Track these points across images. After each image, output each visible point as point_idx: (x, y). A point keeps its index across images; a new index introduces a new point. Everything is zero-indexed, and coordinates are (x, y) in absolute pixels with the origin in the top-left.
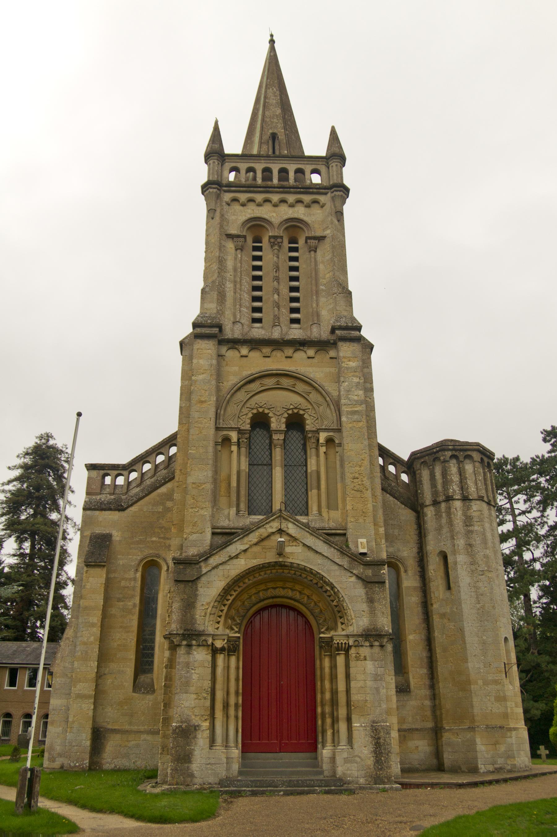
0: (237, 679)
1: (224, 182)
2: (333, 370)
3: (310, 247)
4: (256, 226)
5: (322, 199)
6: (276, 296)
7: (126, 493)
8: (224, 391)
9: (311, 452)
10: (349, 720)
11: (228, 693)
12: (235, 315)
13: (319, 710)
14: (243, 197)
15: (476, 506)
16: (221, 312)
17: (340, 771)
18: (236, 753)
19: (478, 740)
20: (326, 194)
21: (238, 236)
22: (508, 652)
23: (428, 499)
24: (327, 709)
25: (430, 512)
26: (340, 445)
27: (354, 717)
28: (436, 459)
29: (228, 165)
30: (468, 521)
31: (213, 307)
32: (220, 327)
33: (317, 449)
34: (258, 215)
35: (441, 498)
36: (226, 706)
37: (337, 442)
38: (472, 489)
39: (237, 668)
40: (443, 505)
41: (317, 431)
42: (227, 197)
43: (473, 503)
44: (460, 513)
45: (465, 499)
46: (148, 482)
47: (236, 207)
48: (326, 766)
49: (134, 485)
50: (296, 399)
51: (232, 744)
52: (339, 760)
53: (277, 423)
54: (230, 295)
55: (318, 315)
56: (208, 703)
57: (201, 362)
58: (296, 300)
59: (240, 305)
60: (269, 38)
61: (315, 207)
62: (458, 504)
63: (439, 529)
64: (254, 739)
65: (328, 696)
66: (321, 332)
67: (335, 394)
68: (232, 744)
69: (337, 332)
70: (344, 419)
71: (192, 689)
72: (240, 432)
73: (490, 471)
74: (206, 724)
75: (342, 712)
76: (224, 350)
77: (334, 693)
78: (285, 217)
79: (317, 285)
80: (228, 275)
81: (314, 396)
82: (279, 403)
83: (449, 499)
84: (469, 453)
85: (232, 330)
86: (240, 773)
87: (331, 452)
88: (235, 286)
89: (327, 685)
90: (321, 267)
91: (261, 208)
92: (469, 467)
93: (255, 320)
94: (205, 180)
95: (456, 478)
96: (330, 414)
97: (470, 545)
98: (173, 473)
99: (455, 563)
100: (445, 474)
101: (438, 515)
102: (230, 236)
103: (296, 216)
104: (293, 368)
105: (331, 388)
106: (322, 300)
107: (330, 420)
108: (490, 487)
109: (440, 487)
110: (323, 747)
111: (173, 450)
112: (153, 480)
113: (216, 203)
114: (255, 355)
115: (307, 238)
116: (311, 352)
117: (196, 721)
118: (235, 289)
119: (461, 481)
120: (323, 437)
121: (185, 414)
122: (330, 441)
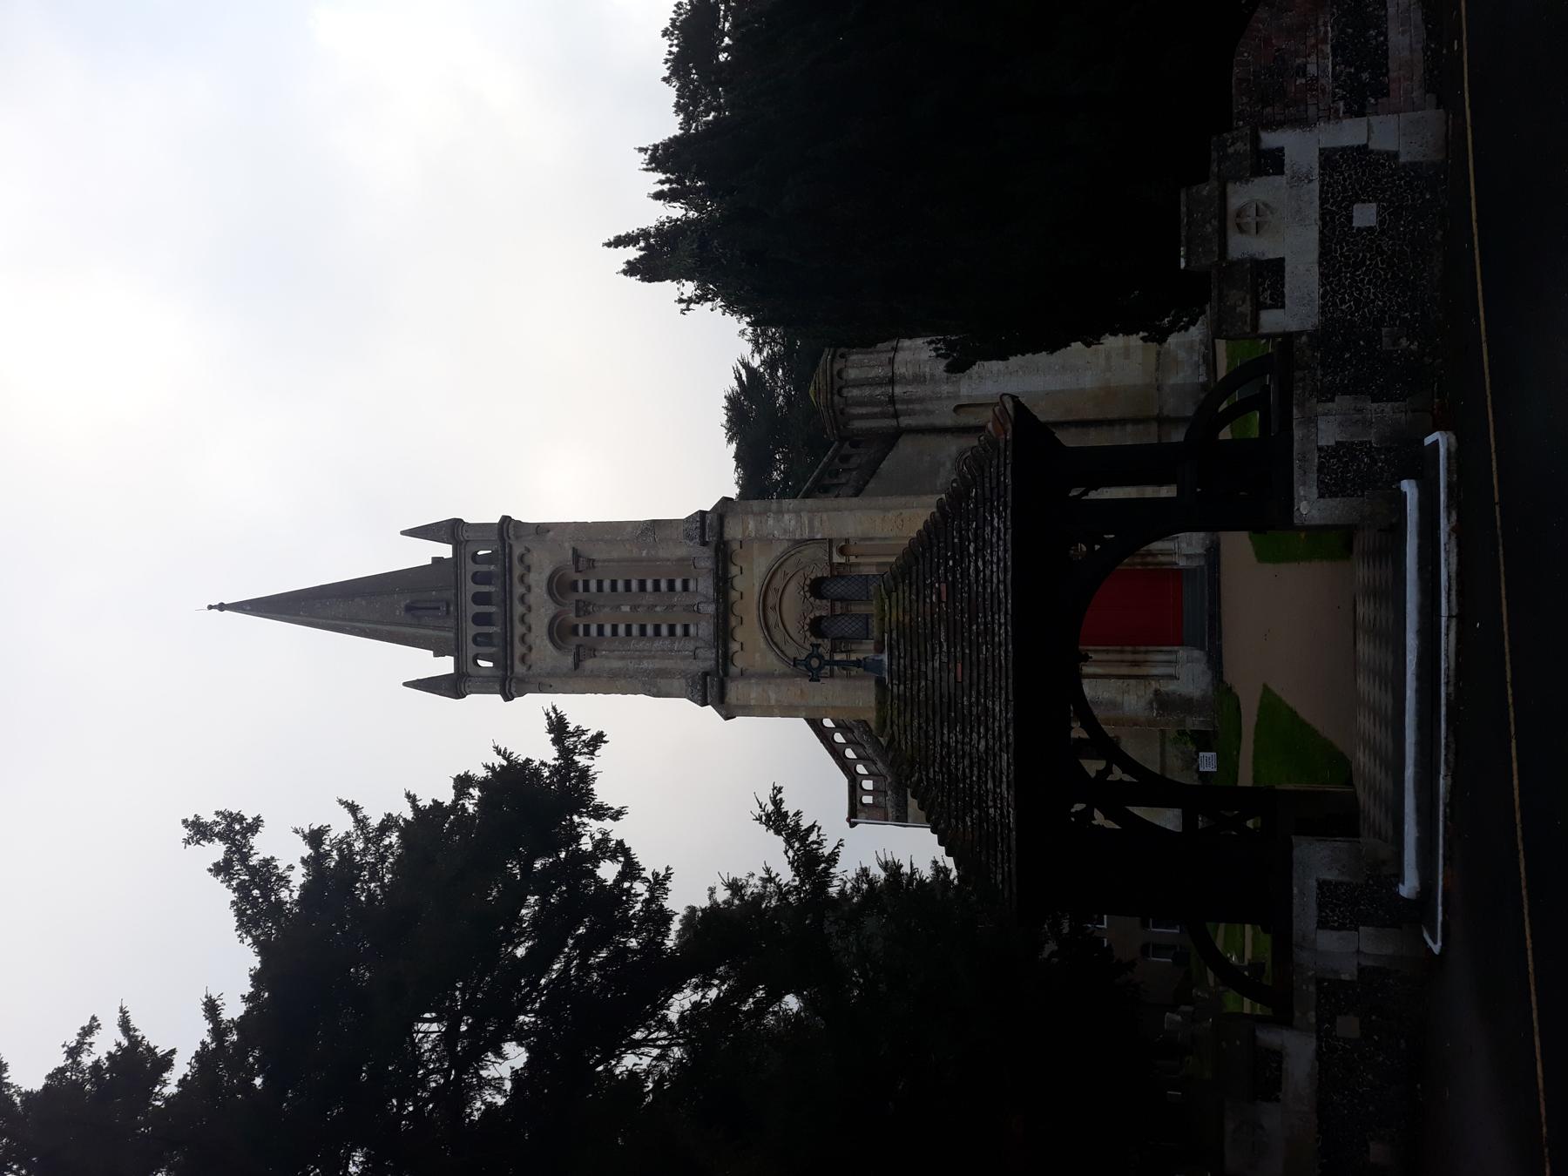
0: (1107, 652)
1: (500, 673)
2: (756, 546)
4: (559, 633)
5: (517, 551)
9: (855, 571)
12: (686, 658)
14: (519, 649)
15: (900, 370)
16: (684, 674)
17: (1201, 551)
18: (1182, 653)
19: (1171, 382)
23: (894, 422)
25: (905, 421)
26: (847, 540)
28: (842, 412)
29: (471, 669)
31: (679, 683)
32: (706, 674)
33: (851, 565)
34: (545, 630)
36: (1135, 663)
38: (880, 372)
40: (898, 407)
41: (832, 565)
42: (519, 669)
43: (897, 372)
44: (910, 388)
45: (892, 381)
47: (533, 656)
48: (1194, 564)
49: (873, 768)
51: (1172, 657)
52: (1190, 551)
53: (822, 608)
54: (657, 664)
56: (1133, 682)
57: (753, 695)
61: (528, 559)
62: (898, 390)
63: (929, 413)
64: (1169, 635)
66: (705, 559)
67: (786, 544)
68: (1172, 657)
71: (1119, 699)
76: (733, 670)
78: (546, 596)
79: (641, 560)
80: (631, 666)
81: (789, 568)
82: (794, 606)
83: (892, 400)
85: (705, 659)
86: (1202, 648)
90: (615, 555)
92: (852, 374)
93: (686, 633)
94: (499, 697)
95: (867, 391)
96: (808, 552)
98: (859, 722)
99: (969, 397)
101: (910, 413)
102: (576, 666)
103: (544, 584)
104: (757, 589)
105: (778, 549)
106: (662, 554)
107: (821, 554)
109: (877, 410)
114: (739, 634)
115: (577, 571)
116: (734, 570)
117: (1150, 695)
120: (837, 559)
121: (788, 711)
122: (842, 551)
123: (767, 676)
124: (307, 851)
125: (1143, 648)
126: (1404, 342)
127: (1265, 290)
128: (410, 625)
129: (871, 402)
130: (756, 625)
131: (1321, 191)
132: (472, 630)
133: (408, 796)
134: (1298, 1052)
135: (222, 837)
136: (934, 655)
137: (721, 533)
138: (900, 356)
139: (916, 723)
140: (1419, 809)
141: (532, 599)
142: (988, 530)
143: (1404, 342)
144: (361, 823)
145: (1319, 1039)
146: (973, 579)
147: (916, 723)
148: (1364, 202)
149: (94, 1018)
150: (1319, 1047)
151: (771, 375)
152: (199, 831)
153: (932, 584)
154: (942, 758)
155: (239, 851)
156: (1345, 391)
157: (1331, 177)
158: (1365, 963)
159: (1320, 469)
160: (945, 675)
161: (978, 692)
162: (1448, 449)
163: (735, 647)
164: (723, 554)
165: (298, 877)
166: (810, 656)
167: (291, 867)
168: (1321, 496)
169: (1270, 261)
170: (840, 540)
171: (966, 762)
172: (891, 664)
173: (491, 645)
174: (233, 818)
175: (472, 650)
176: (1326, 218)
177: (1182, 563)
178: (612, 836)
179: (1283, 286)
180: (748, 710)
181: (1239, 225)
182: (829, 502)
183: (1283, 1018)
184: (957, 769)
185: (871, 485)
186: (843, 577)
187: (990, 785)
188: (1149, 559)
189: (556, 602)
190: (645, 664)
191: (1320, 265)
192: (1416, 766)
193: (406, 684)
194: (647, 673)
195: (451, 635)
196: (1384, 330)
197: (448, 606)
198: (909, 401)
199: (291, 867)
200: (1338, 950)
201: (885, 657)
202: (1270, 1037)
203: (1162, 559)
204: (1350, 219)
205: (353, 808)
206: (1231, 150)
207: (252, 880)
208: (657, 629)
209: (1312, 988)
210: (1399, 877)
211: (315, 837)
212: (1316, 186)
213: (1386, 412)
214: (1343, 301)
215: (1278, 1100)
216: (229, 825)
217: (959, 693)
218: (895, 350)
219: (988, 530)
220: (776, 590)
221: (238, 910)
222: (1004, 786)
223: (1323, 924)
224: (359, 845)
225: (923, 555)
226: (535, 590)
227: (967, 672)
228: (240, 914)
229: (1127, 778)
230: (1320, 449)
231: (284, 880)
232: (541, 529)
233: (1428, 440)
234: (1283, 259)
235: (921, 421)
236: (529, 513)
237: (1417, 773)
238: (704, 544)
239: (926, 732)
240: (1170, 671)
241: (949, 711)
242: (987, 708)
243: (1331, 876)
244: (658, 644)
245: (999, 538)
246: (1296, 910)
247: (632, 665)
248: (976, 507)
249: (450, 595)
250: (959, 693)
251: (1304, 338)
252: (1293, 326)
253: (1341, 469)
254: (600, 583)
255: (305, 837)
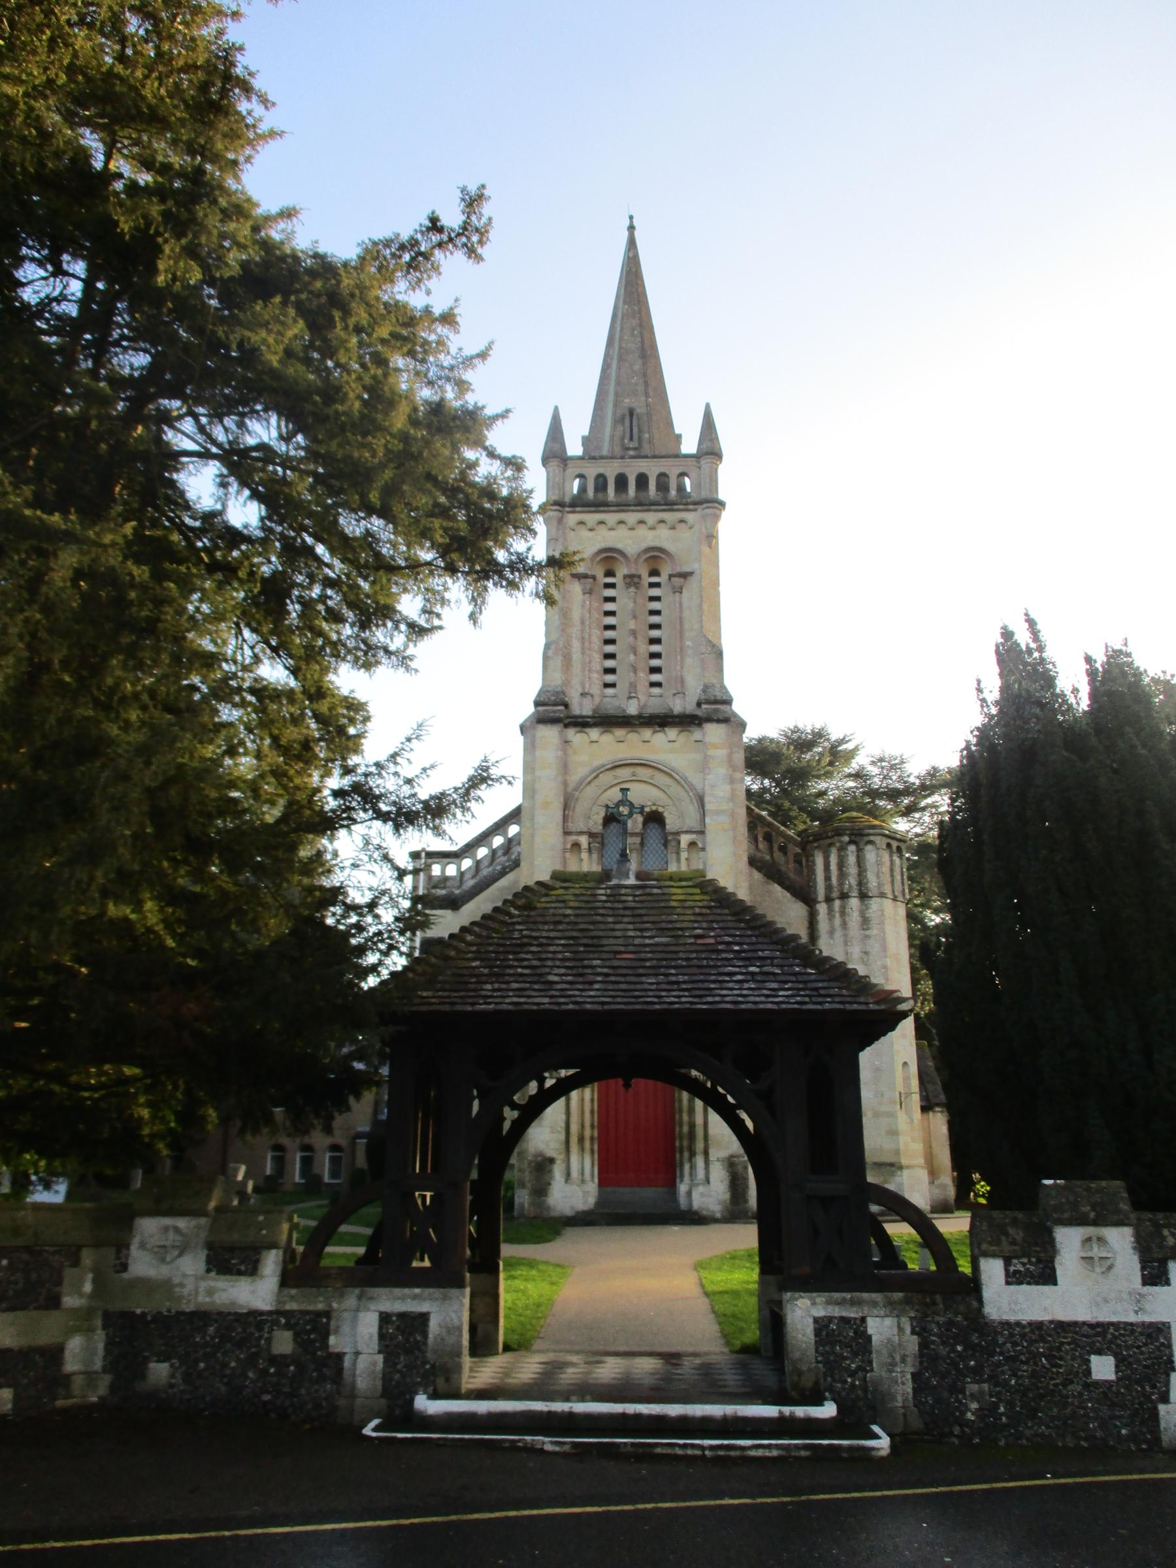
0: (592, 1112)
1: (567, 499)
3: (674, 588)
5: (689, 517)
6: (632, 657)
7: (459, 887)
8: (571, 786)
10: (706, 1153)
11: (583, 1126)
13: (677, 1144)
15: (874, 904)
16: (566, 683)
18: (592, 1187)
20: (695, 510)
21: (586, 576)
22: (906, 1079)
24: (685, 1143)
25: (822, 908)
26: (703, 849)
27: (711, 1151)
29: (572, 471)
30: (865, 922)
31: (557, 679)
32: (566, 706)
33: (678, 853)
35: (835, 894)
36: (581, 1140)
37: (700, 845)
39: (592, 1100)
40: (837, 903)
41: (678, 833)
42: (572, 519)
45: (864, 896)
46: (485, 872)
47: (584, 533)
49: (468, 876)
50: (655, 793)
52: (695, 1195)
54: (576, 656)
55: (682, 681)
56: (562, 1137)
58: (657, 655)
59: (590, 671)
60: (627, 223)
62: (854, 902)
63: (831, 932)
65: (686, 1129)
67: (699, 787)
69: (704, 706)
70: (707, 820)
72: (591, 835)
73: (901, 856)
74: (562, 1157)
75: (700, 1145)
76: (571, 733)
77: (692, 1126)
78: (644, 545)
81: (675, 789)
83: (844, 896)
84: (872, 838)
85: (581, 705)
87: (694, 855)
88: (583, 643)
89: (685, 1118)
91: (612, 533)
95: (852, 870)
96: (692, 811)
97: (866, 953)
100: (841, 865)
101: (830, 911)
104: (652, 757)
105: (695, 779)
106: (689, 661)
107: (692, 821)
108: (898, 877)
110: (682, 1181)
111: (513, 830)
112: (490, 869)
113: (558, 529)
115: (671, 576)
117: (550, 1153)
118: (583, 649)
119: (860, 874)
120: (685, 839)
122: (692, 844)
123: (565, 767)
124: (437, 311)
125: (596, 1147)
126: (974, 1406)
127: (1024, 1264)
128: (614, 414)
129: (842, 875)
130: (621, 756)
131: (1126, 1324)
132: (611, 473)
133: (508, 411)
134: (257, 1292)
135: (465, 227)
136: (641, 930)
137: (709, 720)
138: (888, 904)
139: (569, 912)
140: (503, 1415)
141: (642, 531)
142: (774, 985)
143: (974, 1406)
144: (468, 362)
145: (270, 1313)
146: (722, 970)
147: (569, 912)
148: (1117, 1366)
149: (274, 104)
150: (262, 1313)
151: (850, 775)
152: (473, 201)
153: (713, 929)
154: (536, 938)
155: (451, 240)
156: (924, 1345)
157: (1141, 1334)
158: (347, 1362)
159: (844, 1320)
160: (620, 941)
161: (607, 975)
162: (873, 1449)
163: (594, 733)
164: (688, 721)
165: (416, 300)
166: (631, 805)
167: (428, 293)
168: (816, 1320)
169: (1054, 1270)
170: (704, 843)
171: (535, 963)
172: (626, 887)
173: (597, 490)
174: (483, 233)
175: (591, 472)
176: (1099, 1328)
177: (683, 1188)
178: (446, 608)
179: (1029, 1283)
180: (530, 747)
181: (1089, 1240)
182: (743, 829)
183: (294, 1276)
184: (526, 953)
185: (757, 875)
186: (666, 844)
187: (515, 986)
188: (686, 1155)
189: (639, 555)
190: (576, 645)
191: (1051, 1322)
192: (550, 1412)
193: (556, 409)
194: (568, 645)
195: (605, 453)
196: (985, 1386)
197: (635, 449)
198: (843, 913)
199: (428, 293)
200: (359, 1334)
201: (632, 881)
202: (271, 1263)
203: (687, 1167)
204: (1099, 1352)
205: (483, 356)
206: (1166, 1232)
207: (420, 254)
208: (611, 656)
209: (320, 1306)
210: (435, 1396)
211: (448, 319)
212: (1132, 1318)
213: (904, 1389)
214: (1015, 1344)
215: (208, 1271)
216: (477, 230)
217: (604, 956)
218: (895, 899)
219: (774, 985)
220: (652, 777)
221: (392, 241)
222: (515, 1000)
223: (385, 1318)
224: (446, 361)
225: (740, 921)
226: (651, 534)
227: (628, 963)
228: (387, 243)
229: (507, 1125)
230: (863, 1320)
231: (416, 285)
232: (711, 538)
233: (876, 1429)
234: (1055, 1283)
235: (823, 925)
236: (727, 526)
237: (541, 1413)
238: (699, 704)
239: (560, 923)
240: (575, 1173)
241: (585, 945)
242: (591, 983)
243: (434, 1325)
244: (597, 657)
245: (767, 996)
246: (398, 1291)
247: (575, 631)
248: (795, 974)
249: (647, 449)
250: (604, 956)
251: (975, 1304)
252: (987, 1294)
253: (843, 1341)
254: (658, 599)
255: (451, 309)
